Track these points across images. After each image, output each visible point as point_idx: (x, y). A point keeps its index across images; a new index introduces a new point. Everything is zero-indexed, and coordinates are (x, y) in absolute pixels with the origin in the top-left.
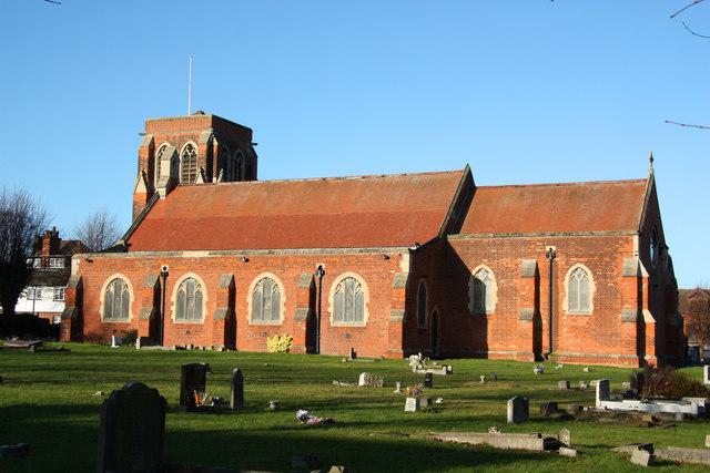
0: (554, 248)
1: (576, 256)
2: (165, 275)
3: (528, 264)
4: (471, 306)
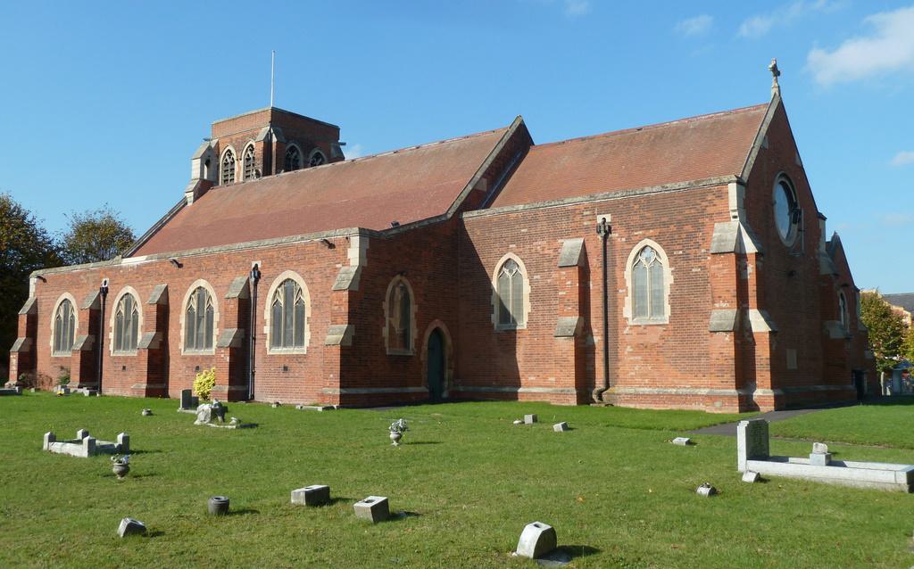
0: (609, 218)
1: (642, 227)
2: (104, 292)
3: (570, 247)
4: (495, 318)
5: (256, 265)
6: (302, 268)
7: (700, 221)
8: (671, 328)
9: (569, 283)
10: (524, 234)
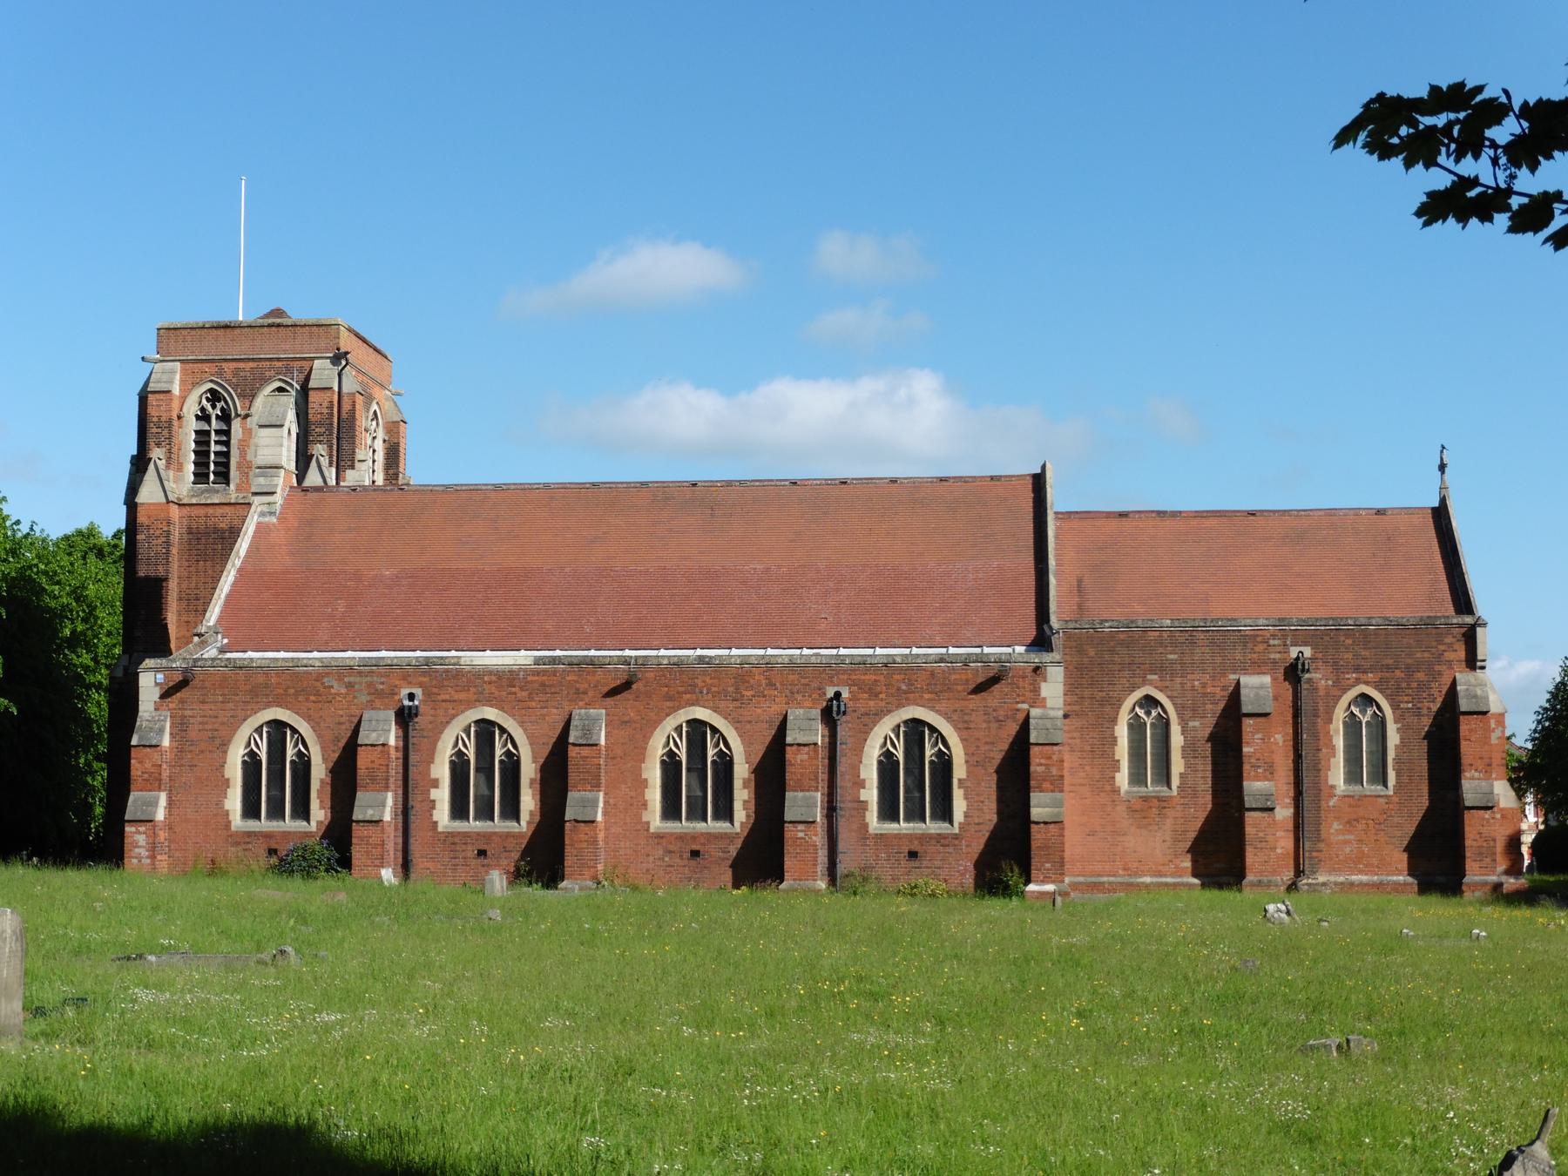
0: (1308, 652)
1: (1357, 669)
5: (838, 695)
6: (943, 705)
7: (1437, 668)
8: (1396, 799)
9: (1259, 736)
10: (1172, 662)
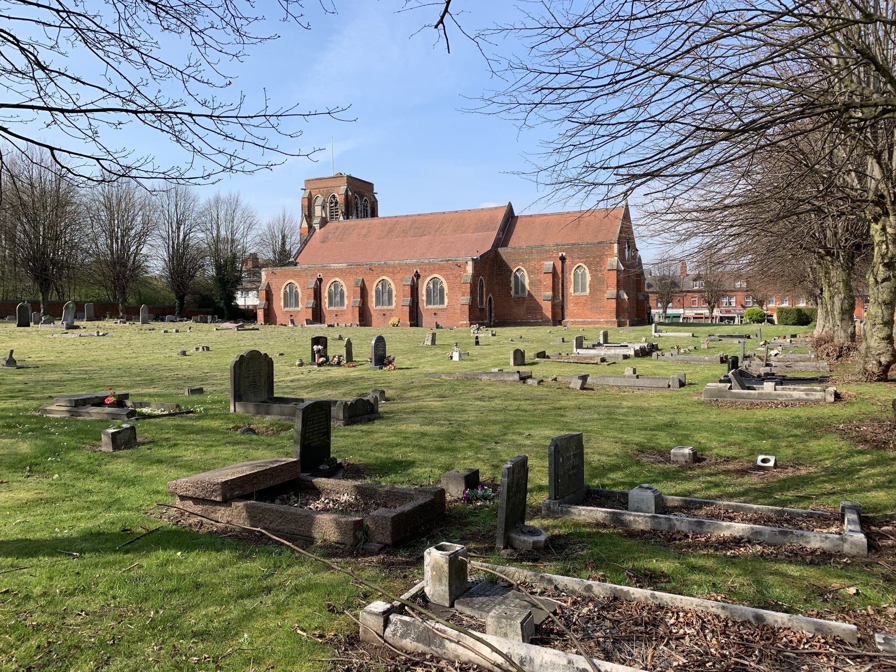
0: (564, 254)
1: (579, 258)
2: (320, 280)
3: (548, 265)
